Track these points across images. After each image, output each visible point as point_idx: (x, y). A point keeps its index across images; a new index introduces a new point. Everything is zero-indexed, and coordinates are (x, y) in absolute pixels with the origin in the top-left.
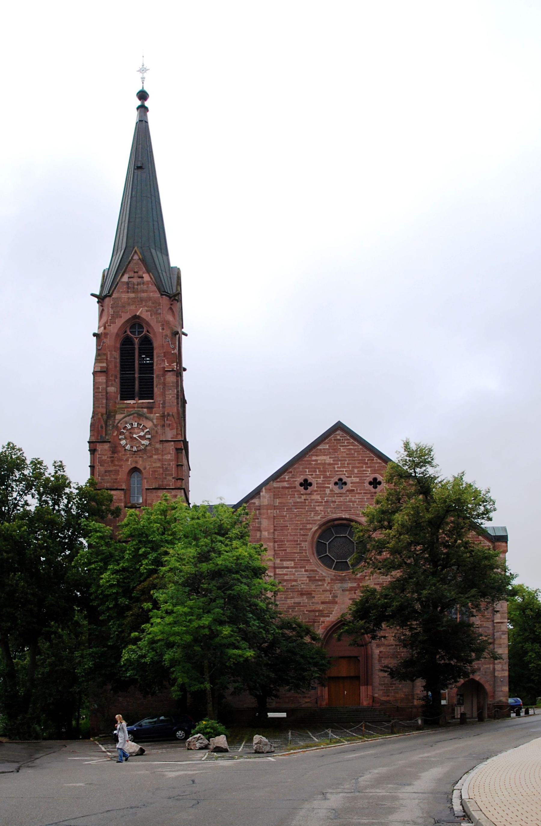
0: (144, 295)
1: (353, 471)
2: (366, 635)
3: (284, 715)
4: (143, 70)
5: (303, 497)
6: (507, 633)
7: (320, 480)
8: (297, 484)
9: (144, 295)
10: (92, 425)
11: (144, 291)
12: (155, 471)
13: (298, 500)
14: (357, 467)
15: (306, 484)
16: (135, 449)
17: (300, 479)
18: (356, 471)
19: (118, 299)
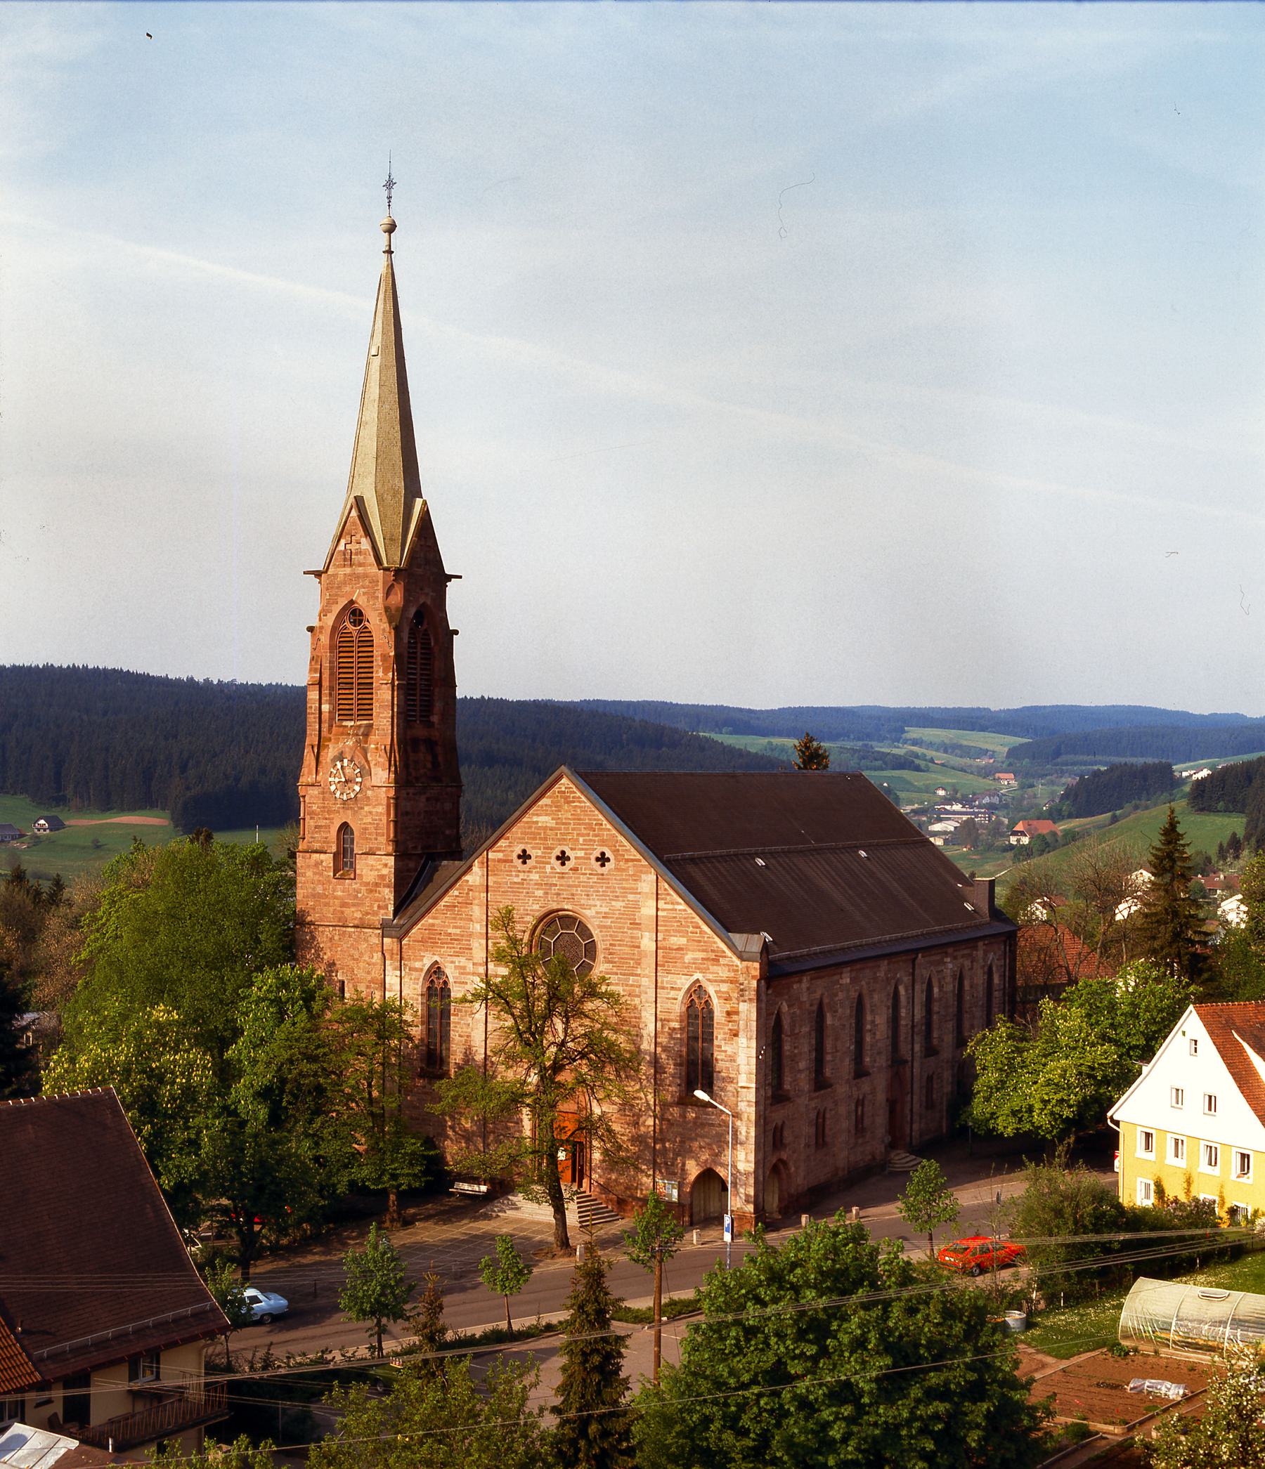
0: (360, 570)
1: (577, 840)
2: (251, 1271)
3: (484, 1188)
4: (391, 228)
5: (522, 876)
6: (1008, 912)
7: (539, 853)
8: (515, 856)
9: (360, 570)
10: (1036, 708)
11: (360, 565)
12: (366, 829)
13: (516, 880)
14: (583, 835)
15: (524, 857)
16: (345, 798)
17: (518, 850)
18: (581, 839)
19: (335, 575)
